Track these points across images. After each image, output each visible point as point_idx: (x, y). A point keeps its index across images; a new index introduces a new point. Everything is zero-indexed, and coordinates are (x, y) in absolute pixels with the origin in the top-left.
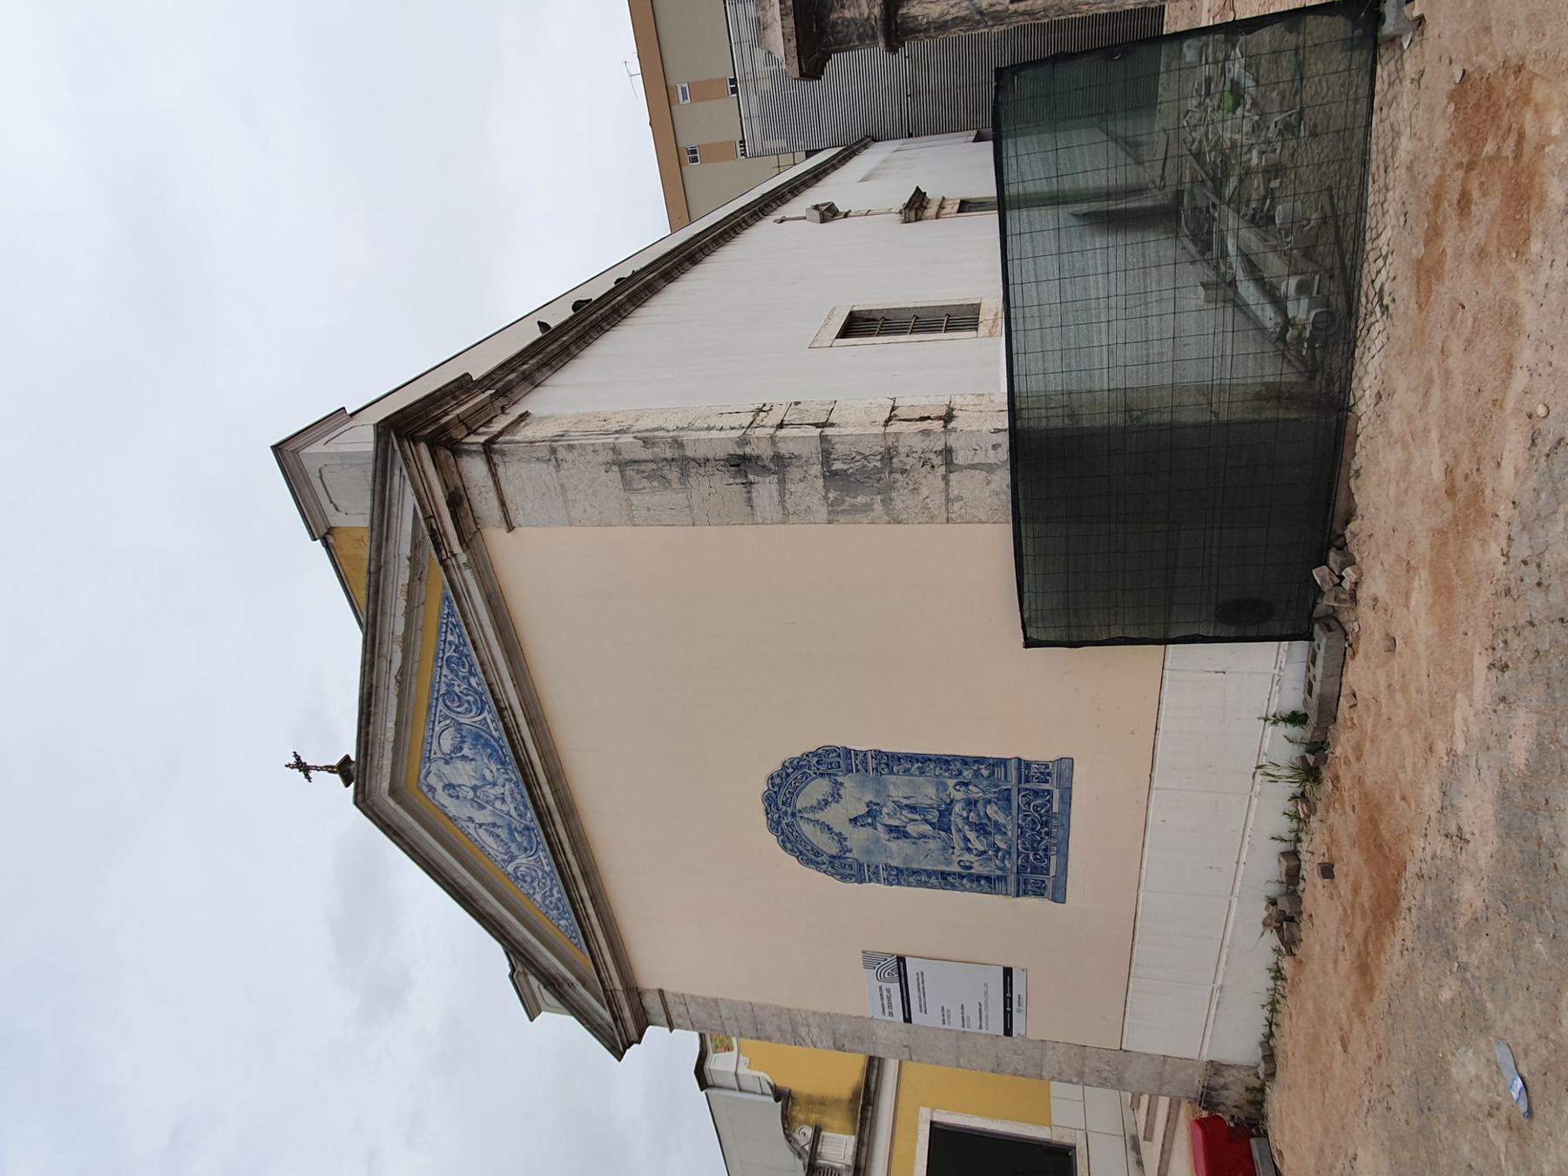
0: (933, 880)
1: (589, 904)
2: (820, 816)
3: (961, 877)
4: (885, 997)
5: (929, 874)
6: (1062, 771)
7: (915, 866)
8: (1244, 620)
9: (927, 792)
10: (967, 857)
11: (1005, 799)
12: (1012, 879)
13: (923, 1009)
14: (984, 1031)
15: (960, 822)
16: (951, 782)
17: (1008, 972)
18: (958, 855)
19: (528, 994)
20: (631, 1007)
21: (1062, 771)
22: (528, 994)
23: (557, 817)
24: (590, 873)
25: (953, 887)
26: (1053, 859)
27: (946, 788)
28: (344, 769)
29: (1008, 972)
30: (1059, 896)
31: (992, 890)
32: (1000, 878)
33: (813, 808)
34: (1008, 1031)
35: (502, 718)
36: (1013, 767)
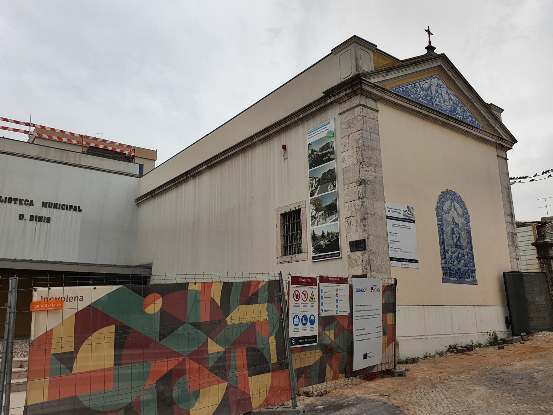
0: (442, 240)
1: (419, 110)
2: (453, 208)
3: (444, 249)
4: (397, 211)
5: (443, 239)
6: (474, 282)
7: (445, 235)
8: (508, 322)
9: (464, 243)
10: (450, 252)
11: (466, 266)
12: (446, 266)
13: (394, 225)
14: (390, 249)
15: (458, 251)
16: (467, 250)
17: (417, 261)
18: (450, 250)
19: (367, 46)
20: (375, 95)
21: (474, 282)
22: (367, 46)
23: (446, 121)
24: (425, 117)
25: (441, 246)
26: (454, 279)
27: (466, 248)
28: (430, 48)
29: (417, 261)
30: (444, 281)
31: (442, 259)
32: (446, 262)
33: (454, 207)
34: (392, 259)
35: (471, 126)
36: (472, 268)
